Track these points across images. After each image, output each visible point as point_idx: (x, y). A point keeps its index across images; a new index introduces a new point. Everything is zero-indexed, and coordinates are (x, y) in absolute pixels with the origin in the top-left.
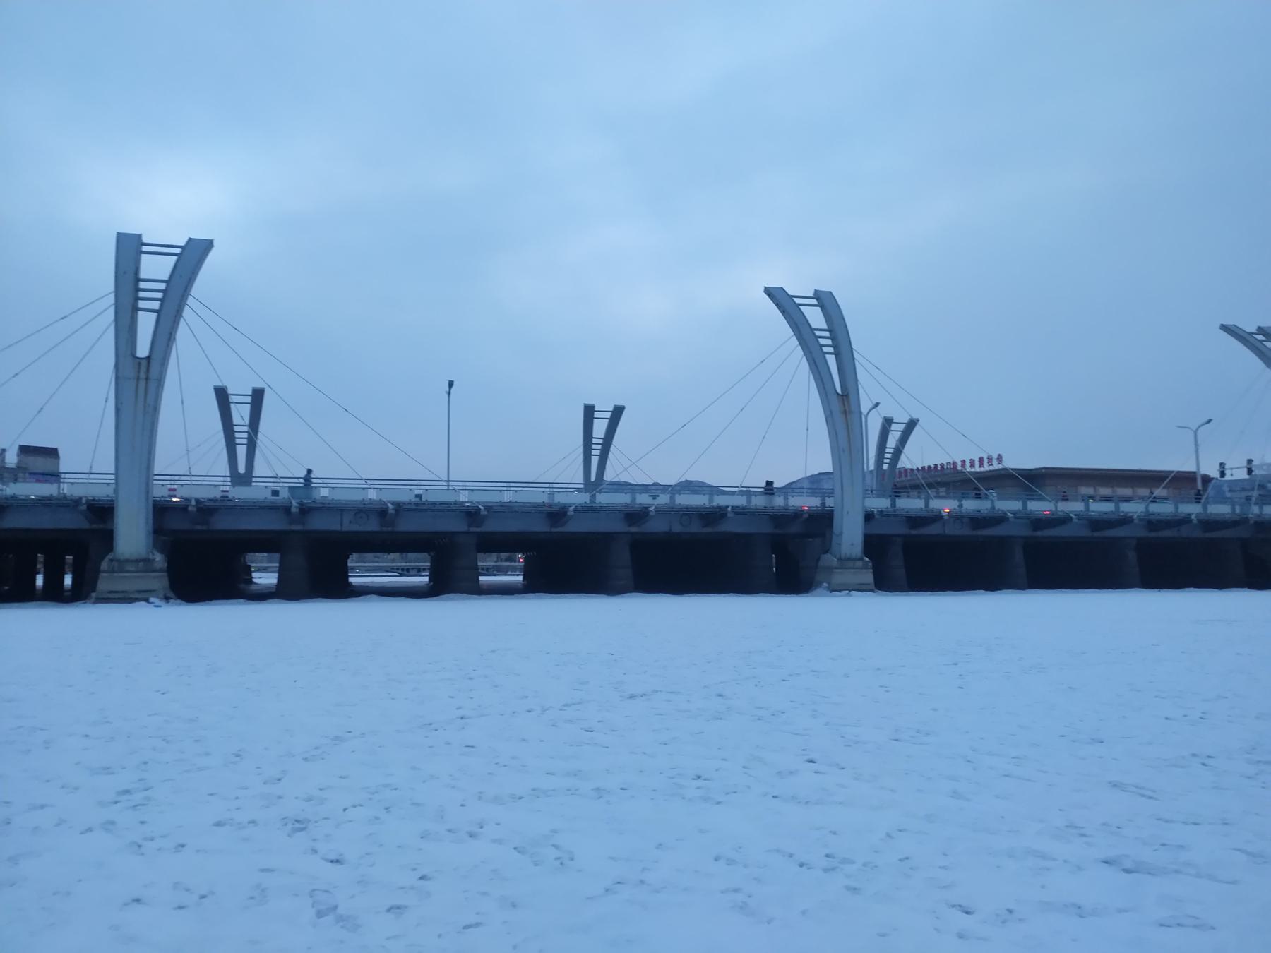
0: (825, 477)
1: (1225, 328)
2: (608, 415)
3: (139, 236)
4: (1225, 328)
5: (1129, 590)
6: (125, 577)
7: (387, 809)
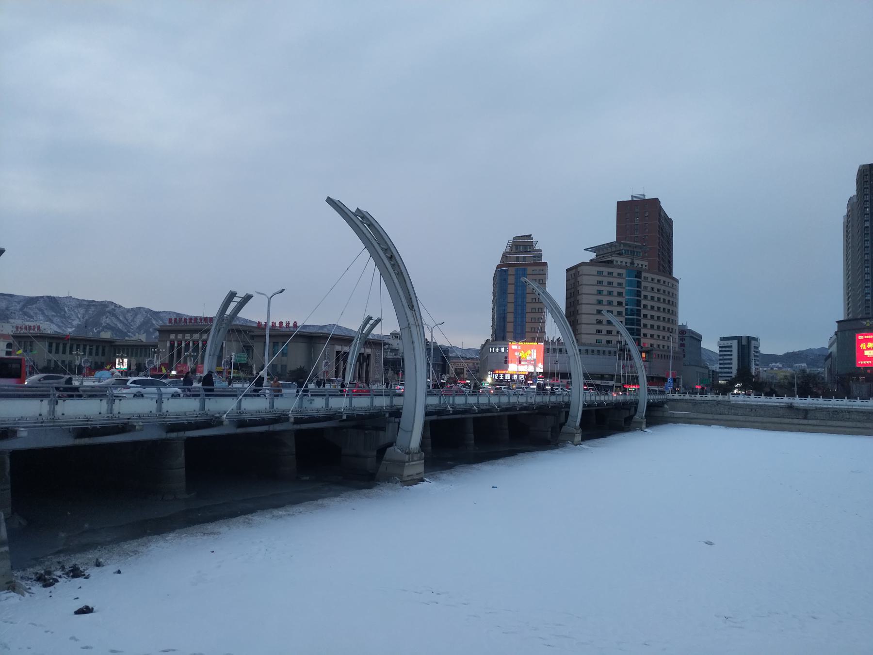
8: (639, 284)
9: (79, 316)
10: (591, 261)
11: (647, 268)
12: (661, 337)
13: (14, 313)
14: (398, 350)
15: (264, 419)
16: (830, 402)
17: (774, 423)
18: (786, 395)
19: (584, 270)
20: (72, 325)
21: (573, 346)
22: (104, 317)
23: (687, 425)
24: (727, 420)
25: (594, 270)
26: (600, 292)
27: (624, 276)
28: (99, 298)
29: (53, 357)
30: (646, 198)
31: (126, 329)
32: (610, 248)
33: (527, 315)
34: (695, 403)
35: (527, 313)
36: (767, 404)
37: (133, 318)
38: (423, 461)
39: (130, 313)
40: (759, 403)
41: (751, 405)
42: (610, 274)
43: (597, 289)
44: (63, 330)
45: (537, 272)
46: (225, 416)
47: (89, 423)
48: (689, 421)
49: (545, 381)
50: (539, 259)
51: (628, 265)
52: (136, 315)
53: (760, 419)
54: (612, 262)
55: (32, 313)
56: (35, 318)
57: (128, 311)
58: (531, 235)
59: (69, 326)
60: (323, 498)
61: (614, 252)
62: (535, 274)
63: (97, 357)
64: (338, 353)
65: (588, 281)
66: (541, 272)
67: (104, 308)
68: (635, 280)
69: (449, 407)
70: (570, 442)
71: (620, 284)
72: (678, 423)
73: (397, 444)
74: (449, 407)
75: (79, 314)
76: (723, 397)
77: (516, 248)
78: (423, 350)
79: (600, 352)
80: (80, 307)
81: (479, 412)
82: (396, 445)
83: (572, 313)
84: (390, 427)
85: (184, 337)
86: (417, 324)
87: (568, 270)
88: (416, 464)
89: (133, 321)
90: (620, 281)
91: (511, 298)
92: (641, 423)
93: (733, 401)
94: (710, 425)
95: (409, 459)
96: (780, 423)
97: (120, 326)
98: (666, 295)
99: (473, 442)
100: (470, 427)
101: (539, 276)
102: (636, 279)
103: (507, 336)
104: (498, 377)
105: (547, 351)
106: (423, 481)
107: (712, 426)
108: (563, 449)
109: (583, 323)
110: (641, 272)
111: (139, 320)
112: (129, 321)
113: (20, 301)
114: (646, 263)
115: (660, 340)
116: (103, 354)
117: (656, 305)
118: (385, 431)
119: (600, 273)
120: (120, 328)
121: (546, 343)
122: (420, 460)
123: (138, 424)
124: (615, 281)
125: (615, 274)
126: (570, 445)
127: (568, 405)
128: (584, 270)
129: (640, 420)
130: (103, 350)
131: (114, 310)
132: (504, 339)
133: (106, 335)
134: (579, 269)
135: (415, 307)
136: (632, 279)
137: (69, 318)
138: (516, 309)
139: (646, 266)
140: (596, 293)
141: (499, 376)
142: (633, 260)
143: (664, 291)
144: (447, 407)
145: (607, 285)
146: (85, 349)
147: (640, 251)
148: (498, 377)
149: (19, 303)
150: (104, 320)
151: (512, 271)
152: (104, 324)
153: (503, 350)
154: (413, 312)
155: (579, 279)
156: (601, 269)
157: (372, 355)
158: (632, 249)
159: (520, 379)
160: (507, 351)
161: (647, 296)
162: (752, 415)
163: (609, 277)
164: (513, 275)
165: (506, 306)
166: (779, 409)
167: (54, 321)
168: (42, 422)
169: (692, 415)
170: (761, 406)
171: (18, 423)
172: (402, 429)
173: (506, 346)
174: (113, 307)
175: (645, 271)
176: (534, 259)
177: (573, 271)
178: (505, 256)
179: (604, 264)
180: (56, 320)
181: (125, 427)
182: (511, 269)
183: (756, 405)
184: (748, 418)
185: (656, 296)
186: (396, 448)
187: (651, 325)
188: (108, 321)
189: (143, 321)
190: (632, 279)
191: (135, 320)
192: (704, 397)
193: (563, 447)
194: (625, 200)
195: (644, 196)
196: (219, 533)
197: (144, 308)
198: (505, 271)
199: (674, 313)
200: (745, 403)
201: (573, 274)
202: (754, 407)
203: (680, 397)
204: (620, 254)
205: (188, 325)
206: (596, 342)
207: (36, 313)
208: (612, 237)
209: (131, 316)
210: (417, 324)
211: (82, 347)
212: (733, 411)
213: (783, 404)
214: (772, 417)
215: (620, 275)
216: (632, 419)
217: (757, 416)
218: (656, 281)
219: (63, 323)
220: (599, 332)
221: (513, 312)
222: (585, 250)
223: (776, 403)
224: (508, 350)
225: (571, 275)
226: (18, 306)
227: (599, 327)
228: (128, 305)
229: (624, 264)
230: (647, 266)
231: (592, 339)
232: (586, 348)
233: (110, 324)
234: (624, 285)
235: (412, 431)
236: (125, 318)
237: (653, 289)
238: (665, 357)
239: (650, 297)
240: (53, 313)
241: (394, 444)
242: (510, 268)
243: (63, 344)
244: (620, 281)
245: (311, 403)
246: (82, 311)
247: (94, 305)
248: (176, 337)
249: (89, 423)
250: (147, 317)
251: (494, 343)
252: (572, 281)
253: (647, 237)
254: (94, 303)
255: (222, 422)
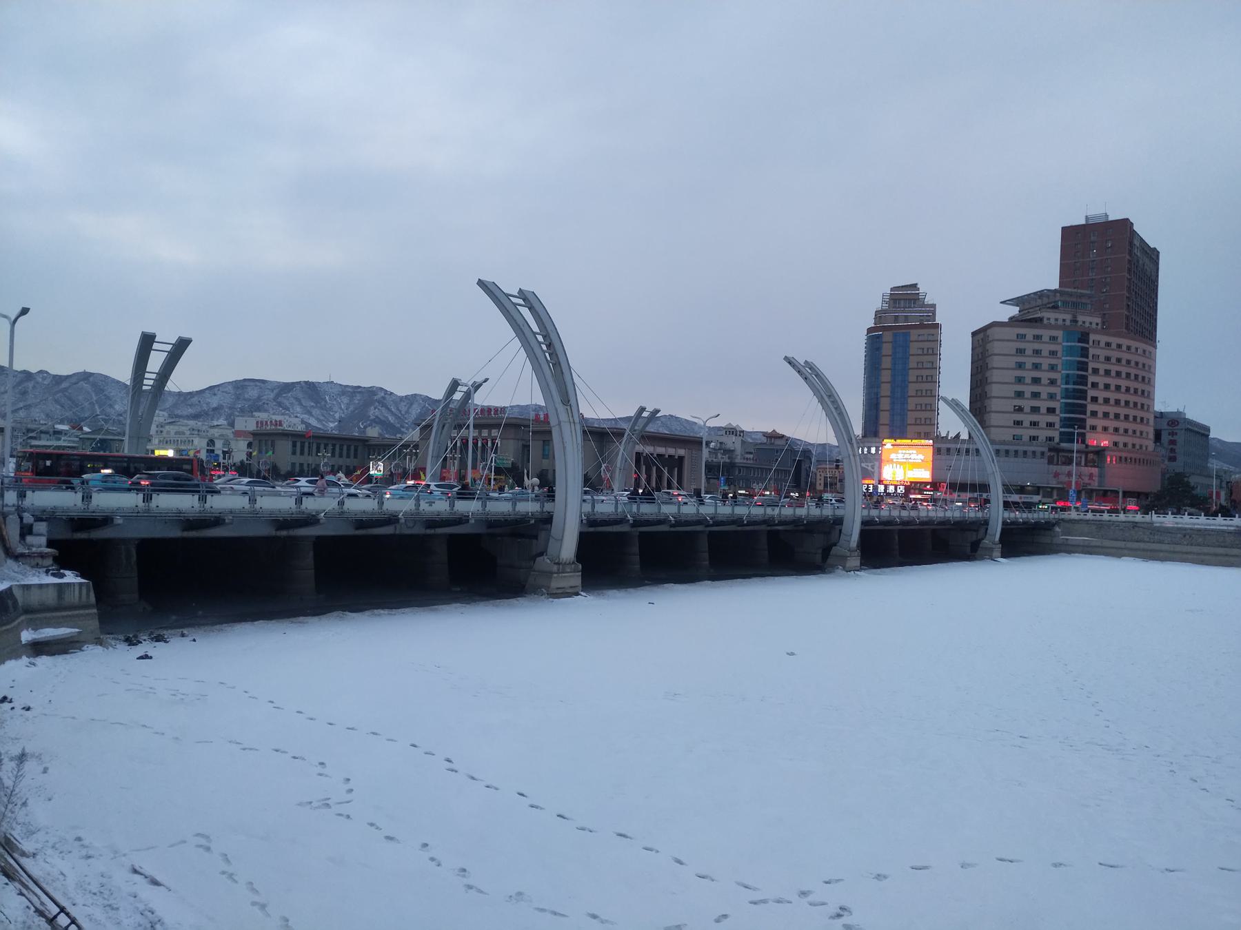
0: (252, 384)
1: (481, 283)
2: (169, 348)
3: (1208, 429)
4: (481, 283)
5: (1017, 559)
6: (565, 577)
7: (328, 805)
8: (1084, 352)
9: (343, 407)
10: (1011, 319)
11: (1099, 327)
12: (1130, 432)
13: (267, 404)
14: (733, 451)
15: (362, 520)
16: (1231, 523)
17: (1216, 555)
18: (1220, 515)
19: (996, 333)
20: (334, 418)
21: (848, 444)
22: (372, 407)
23: (1087, 556)
24: (1147, 550)
25: (1013, 332)
26: (1020, 366)
27: (1060, 340)
28: (366, 383)
29: (298, 459)
30: (1111, 219)
31: (398, 423)
32: (1039, 298)
33: (910, 400)
34: (1100, 525)
35: (909, 397)
36: (1208, 527)
37: (409, 408)
38: (580, 573)
39: (404, 401)
40: (1196, 526)
41: (1185, 529)
42: (1037, 338)
43: (1049, 362)
44: (324, 425)
45: (925, 338)
46: (323, 514)
47: (182, 515)
48: (1088, 550)
49: (935, 495)
50: (927, 318)
51: (1068, 323)
52: (412, 404)
53: (1195, 549)
54: (1041, 319)
55: (288, 405)
56: (291, 409)
57: (402, 399)
58: (916, 284)
59: (331, 419)
60: (438, 604)
61: (1046, 305)
62: (921, 341)
63: (348, 460)
64: (638, 455)
65: (1001, 348)
66: (930, 338)
67: (371, 396)
68: (1078, 346)
69: (629, 516)
70: (841, 567)
71: (1053, 353)
72: (1074, 552)
73: (548, 554)
74: (629, 516)
75: (342, 404)
76: (1094, 515)
77: (895, 303)
78: (578, 450)
79: (1028, 453)
80: (343, 395)
81: (748, 525)
82: (546, 555)
83: (978, 396)
84: (542, 535)
85: (490, 433)
86: (571, 420)
87: (974, 334)
88: (570, 576)
89: (407, 412)
90: (1053, 347)
91: (886, 376)
92: (991, 550)
93: (1157, 523)
94: (1119, 556)
95: (559, 570)
96: (1227, 555)
97: (391, 419)
98: (1131, 367)
99: (707, 563)
100: (704, 544)
101: (926, 343)
102: (1080, 344)
103: (880, 430)
104: (867, 489)
105: (937, 452)
106: (577, 594)
107: (1123, 558)
108: (831, 575)
109: (992, 412)
110: (1088, 334)
111: (415, 411)
112: (403, 413)
113: (274, 388)
114: (1099, 320)
115: (1136, 437)
116: (356, 456)
117: (1113, 382)
118: (537, 539)
119: (1021, 337)
120: (392, 421)
121: (938, 439)
122: (574, 572)
123: (228, 519)
124: (1046, 348)
125: (1046, 338)
126: (840, 571)
127: (839, 521)
128: (996, 333)
129: (991, 545)
130: (356, 450)
131: (384, 398)
132: (876, 434)
133: (373, 432)
134: (989, 332)
135: (573, 402)
136: (1073, 344)
137: (331, 409)
138: (893, 392)
139: (1097, 324)
140: (1014, 367)
141: (868, 487)
142: (1075, 316)
143: (1137, 364)
144: (627, 516)
145: (1048, 355)
146: (334, 450)
147: (1088, 301)
148: (867, 489)
149: (273, 391)
150: (372, 412)
151: (888, 336)
152: (372, 417)
153: (873, 450)
154: (569, 408)
155: (988, 346)
156: (1022, 331)
157: (686, 458)
158: (1074, 300)
159: (899, 491)
160: (880, 452)
161: (1121, 372)
162: (1185, 543)
163: (1052, 343)
164: (912, 341)
165: (879, 387)
166: (1226, 535)
167: (313, 414)
168: (138, 513)
169: (1095, 541)
170: (1199, 530)
171: (117, 513)
172: (553, 538)
173: (878, 445)
174: (383, 394)
175: (1096, 332)
176: (921, 318)
177: (981, 335)
178: (879, 315)
179: (1028, 323)
180: (316, 412)
181: (217, 521)
182: (886, 333)
183: (1191, 529)
184: (1178, 548)
185: (1124, 370)
186: (546, 558)
187: (1125, 415)
188: (377, 412)
189: (420, 412)
190: (1073, 344)
191: (410, 410)
192: (1114, 517)
193: (830, 572)
194: (1074, 224)
195: (1107, 215)
196: (307, 622)
197: (421, 395)
198: (878, 337)
199: (1148, 395)
200: (1176, 526)
201: (982, 338)
202: (1189, 531)
203: (1110, 517)
204: (1055, 307)
205: (493, 418)
206: (1014, 439)
207: (292, 404)
208: (1053, 283)
209: (405, 406)
210: (571, 420)
211: (330, 447)
212: (1156, 537)
213: (1232, 528)
214: (1214, 547)
215: (1053, 339)
216: (980, 543)
217: (1192, 545)
218: (1124, 348)
219: (324, 416)
220: (1018, 423)
221: (889, 397)
222: (1001, 303)
223: (1222, 526)
224: (881, 450)
225: (978, 341)
226: (272, 394)
227: (1019, 417)
228: (401, 391)
229: (1060, 322)
230: (1100, 325)
231: (1007, 435)
232: (1007, 447)
233: (379, 416)
234: (1059, 354)
235: (562, 540)
236: (398, 409)
237: (1119, 360)
238: (1140, 462)
239: (1115, 372)
240: (312, 404)
241: (545, 554)
242: (884, 332)
243: (355, 446)
244: (1053, 347)
245: (431, 505)
246: (345, 400)
247: (360, 392)
248: (490, 433)
249: (182, 515)
250: (425, 406)
251: (866, 439)
252: (979, 350)
253: (1108, 280)
254: (359, 390)
255: (319, 520)
